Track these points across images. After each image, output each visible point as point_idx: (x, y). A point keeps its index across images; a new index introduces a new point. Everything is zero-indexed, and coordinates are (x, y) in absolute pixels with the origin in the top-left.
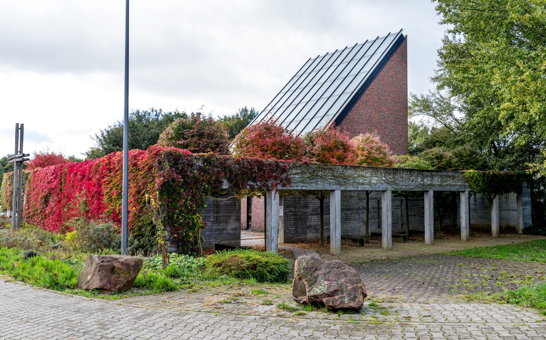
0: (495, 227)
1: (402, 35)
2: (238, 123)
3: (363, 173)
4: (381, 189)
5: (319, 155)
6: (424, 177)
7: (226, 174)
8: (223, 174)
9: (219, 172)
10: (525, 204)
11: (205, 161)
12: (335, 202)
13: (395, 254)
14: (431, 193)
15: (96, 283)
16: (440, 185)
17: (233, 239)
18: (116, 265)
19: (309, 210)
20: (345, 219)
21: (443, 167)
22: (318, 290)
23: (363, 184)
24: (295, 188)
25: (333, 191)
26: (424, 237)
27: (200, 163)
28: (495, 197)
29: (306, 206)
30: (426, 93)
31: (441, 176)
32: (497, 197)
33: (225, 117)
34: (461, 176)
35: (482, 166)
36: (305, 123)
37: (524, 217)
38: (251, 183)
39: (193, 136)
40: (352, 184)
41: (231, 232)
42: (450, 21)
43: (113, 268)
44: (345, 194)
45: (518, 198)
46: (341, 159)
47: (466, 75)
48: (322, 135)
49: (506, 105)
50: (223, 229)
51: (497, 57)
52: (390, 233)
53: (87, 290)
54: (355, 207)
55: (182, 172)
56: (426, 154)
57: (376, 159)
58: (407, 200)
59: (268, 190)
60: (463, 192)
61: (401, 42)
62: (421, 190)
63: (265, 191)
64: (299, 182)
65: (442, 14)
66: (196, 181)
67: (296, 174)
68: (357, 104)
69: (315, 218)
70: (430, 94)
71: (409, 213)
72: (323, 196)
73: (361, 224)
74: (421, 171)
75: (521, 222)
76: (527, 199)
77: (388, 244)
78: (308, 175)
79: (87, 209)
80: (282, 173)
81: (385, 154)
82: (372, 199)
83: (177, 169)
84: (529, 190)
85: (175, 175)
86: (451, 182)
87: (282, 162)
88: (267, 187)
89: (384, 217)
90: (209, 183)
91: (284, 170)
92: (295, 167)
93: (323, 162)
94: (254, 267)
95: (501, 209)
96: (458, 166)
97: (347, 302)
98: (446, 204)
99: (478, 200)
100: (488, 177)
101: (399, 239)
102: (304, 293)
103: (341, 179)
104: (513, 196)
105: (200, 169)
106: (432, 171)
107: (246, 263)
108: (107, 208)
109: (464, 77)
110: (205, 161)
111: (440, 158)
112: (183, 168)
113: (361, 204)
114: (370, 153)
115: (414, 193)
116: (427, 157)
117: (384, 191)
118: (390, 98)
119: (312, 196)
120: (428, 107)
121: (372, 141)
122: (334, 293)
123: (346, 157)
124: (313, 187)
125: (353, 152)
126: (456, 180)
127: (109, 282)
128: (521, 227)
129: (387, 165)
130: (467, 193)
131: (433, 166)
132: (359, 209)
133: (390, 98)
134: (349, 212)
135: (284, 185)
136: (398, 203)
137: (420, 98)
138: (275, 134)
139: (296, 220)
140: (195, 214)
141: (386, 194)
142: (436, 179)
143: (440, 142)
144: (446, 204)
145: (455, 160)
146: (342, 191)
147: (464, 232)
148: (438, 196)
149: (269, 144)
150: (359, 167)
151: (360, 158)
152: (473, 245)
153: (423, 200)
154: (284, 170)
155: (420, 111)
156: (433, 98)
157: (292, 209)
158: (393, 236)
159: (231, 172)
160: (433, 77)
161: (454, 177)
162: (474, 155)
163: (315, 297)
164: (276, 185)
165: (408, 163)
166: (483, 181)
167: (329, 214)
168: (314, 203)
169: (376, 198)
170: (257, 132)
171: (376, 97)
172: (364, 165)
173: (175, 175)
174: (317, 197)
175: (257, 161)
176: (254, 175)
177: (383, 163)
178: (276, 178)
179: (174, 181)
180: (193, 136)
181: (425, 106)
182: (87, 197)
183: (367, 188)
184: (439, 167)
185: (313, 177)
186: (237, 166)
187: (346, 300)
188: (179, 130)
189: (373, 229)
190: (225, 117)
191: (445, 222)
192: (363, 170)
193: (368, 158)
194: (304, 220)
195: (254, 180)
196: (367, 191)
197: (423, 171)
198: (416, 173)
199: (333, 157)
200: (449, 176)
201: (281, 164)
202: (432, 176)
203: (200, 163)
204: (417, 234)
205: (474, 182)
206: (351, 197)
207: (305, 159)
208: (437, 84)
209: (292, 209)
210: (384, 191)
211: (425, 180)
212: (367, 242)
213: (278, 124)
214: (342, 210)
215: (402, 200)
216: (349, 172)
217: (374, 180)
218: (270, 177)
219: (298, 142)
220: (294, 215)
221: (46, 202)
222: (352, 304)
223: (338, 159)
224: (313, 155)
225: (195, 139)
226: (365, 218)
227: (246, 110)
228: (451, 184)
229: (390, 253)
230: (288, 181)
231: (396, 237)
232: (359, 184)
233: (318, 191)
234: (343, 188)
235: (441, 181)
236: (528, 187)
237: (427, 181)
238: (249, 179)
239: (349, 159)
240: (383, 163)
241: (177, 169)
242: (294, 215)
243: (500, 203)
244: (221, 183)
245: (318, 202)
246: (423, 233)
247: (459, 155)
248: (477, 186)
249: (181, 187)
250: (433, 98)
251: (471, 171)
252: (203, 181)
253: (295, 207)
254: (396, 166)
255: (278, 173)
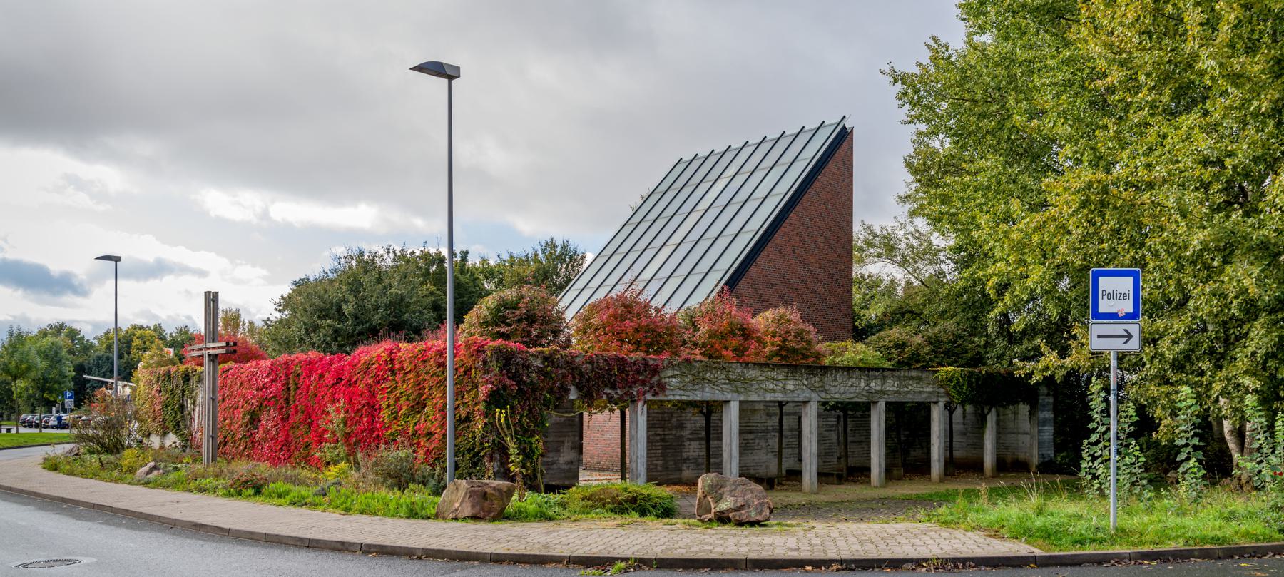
0: (989, 460)
1: (844, 127)
2: (538, 270)
3: (774, 374)
4: (800, 399)
5: (704, 345)
6: (870, 379)
7: (574, 378)
8: (570, 378)
9: (564, 376)
10: (1044, 422)
11: (545, 359)
12: (731, 420)
13: (821, 498)
14: (882, 405)
15: (468, 511)
16: (896, 392)
17: (567, 478)
18: (489, 490)
19: (686, 433)
20: (745, 448)
21: (907, 362)
22: (725, 505)
23: (773, 391)
24: (671, 398)
25: (728, 402)
26: (869, 476)
27: (538, 363)
28: (990, 411)
29: (681, 426)
30: (889, 224)
31: (899, 378)
32: (993, 410)
33: (511, 257)
34: (932, 377)
35: (972, 359)
36: (682, 287)
37: (1041, 444)
38: (608, 390)
39: (520, 321)
40: (756, 392)
41: (564, 467)
42: (918, 118)
43: (486, 493)
44: (745, 407)
45: (1031, 414)
46: (740, 352)
47: (944, 208)
48: (711, 315)
49: (1000, 266)
50: (553, 463)
51: (988, 188)
52: (814, 468)
53: (456, 519)
54: (761, 427)
55: (516, 377)
56: (880, 339)
57: (794, 351)
58: (846, 417)
59: (633, 401)
60: (936, 403)
61: (843, 137)
62: (865, 399)
63: (623, 403)
64: (677, 390)
65: (908, 106)
66: (534, 388)
67: (673, 377)
68: (765, 252)
69: (695, 444)
70: (897, 224)
71: (849, 439)
72: (711, 410)
73: (770, 456)
74: (866, 370)
75: (1035, 452)
76: (1047, 414)
77: (812, 484)
78: (690, 378)
79: (348, 430)
80: (653, 376)
81: (809, 342)
82: (789, 414)
83: (509, 371)
84: (1051, 400)
85: (507, 382)
86: (916, 387)
87: (652, 359)
88: (631, 396)
89: (805, 443)
90: (551, 391)
91: (655, 371)
92: (671, 365)
93: (710, 357)
94: (634, 500)
95: (1000, 431)
96: (931, 360)
97: (753, 516)
98: (908, 424)
99: (969, 417)
100: (977, 379)
101: (831, 479)
102: (709, 511)
103: (739, 384)
104: (1024, 409)
105: (540, 372)
106: (884, 370)
107: (623, 497)
108: (389, 427)
109: (942, 213)
110: (545, 359)
111: (901, 346)
112: (517, 370)
113: (770, 423)
114: (784, 341)
115: (855, 406)
116: (881, 344)
117: (805, 403)
118: (822, 239)
119: (690, 410)
120: (892, 249)
121: (789, 321)
122: (742, 507)
123: (746, 349)
124: (698, 396)
125: (759, 340)
126: (924, 383)
127: (482, 509)
128: (1035, 461)
129: (812, 359)
130: (941, 404)
131: (890, 360)
132: (766, 431)
133: (822, 239)
134: (750, 436)
135: (655, 394)
136: (833, 421)
137: (878, 232)
138: (638, 314)
139: (665, 448)
140: (532, 436)
141: (809, 406)
142: (890, 382)
143: (912, 312)
144: (908, 424)
145: (927, 349)
146: (741, 402)
147: (936, 468)
148: (894, 409)
149: (630, 330)
150: (766, 365)
151: (769, 349)
152: (942, 488)
153: (869, 416)
154: (655, 371)
155: (879, 256)
156: (902, 233)
157: (659, 431)
158: (820, 474)
159: (582, 375)
160: (902, 194)
161: (920, 379)
162: (960, 342)
163: (722, 512)
164: (644, 393)
165: (848, 355)
166: (970, 385)
167: (720, 439)
168: (695, 420)
169: (795, 414)
170: (611, 311)
171: (798, 239)
172: (776, 360)
173: (507, 382)
174: (701, 412)
175: (617, 358)
176: (608, 381)
177: (805, 357)
178: (643, 383)
179: (505, 388)
180: (520, 321)
181: (888, 247)
182: (347, 412)
183: (780, 397)
184: (899, 362)
185: (698, 380)
186: (589, 366)
187: (753, 514)
188: (498, 310)
189: (788, 464)
190: (511, 257)
191: (913, 453)
192: (773, 370)
193: (781, 348)
194: (680, 449)
195: (613, 387)
196: (780, 403)
197: (869, 369)
198: (858, 373)
199: (727, 349)
200: (912, 378)
201: (651, 362)
202: (884, 378)
203: (538, 363)
204: (859, 473)
205: (955, 387)
206: (754, 411)
207: (684, 353)
208: (908, 207)
209: (659, 431)
210: (805, 403)
211: (873, 384)
212: (780, 484)
213: (642, 298)
214: (741, 432)
215: (839, 417)
216: (752, 373)
217: (791, 385)
218: (635, 383)
219: (671, 328)
220: (662, 440)
221: (254, 419)
222: (759, 518)
223: (735, 350)
224: (696, 344)
225: (524, 324)
226: (777, 446)
227: (554, 246)
228: (915, 389)
229: (813, 498)
230: (662, 387)
231: (825, 476)
232: (767, 390)
233: (702, 402)
234: (742, 398)
235: (899, 386)
236: (1048, 395)
237: (875, 386)
238: (606, 385)
239: (752, 350)
240: (805, 357)
241: (509, 371)
242: (662, 440)
243: (998, 423)
244: (567, 391)
245: (701, 421)
246: (869, 469)
247: (934, 342)
248: (960, 393)
249: (515, 398)
250: (902, 233)
251: (950, 368)
252: (543, 388)
253: (663, 428)
254: (827, 361)
255: (647, 376)
